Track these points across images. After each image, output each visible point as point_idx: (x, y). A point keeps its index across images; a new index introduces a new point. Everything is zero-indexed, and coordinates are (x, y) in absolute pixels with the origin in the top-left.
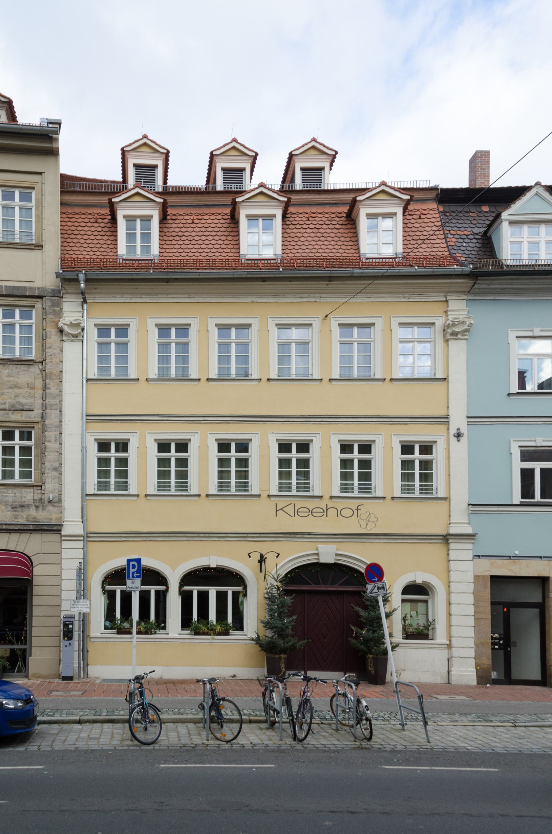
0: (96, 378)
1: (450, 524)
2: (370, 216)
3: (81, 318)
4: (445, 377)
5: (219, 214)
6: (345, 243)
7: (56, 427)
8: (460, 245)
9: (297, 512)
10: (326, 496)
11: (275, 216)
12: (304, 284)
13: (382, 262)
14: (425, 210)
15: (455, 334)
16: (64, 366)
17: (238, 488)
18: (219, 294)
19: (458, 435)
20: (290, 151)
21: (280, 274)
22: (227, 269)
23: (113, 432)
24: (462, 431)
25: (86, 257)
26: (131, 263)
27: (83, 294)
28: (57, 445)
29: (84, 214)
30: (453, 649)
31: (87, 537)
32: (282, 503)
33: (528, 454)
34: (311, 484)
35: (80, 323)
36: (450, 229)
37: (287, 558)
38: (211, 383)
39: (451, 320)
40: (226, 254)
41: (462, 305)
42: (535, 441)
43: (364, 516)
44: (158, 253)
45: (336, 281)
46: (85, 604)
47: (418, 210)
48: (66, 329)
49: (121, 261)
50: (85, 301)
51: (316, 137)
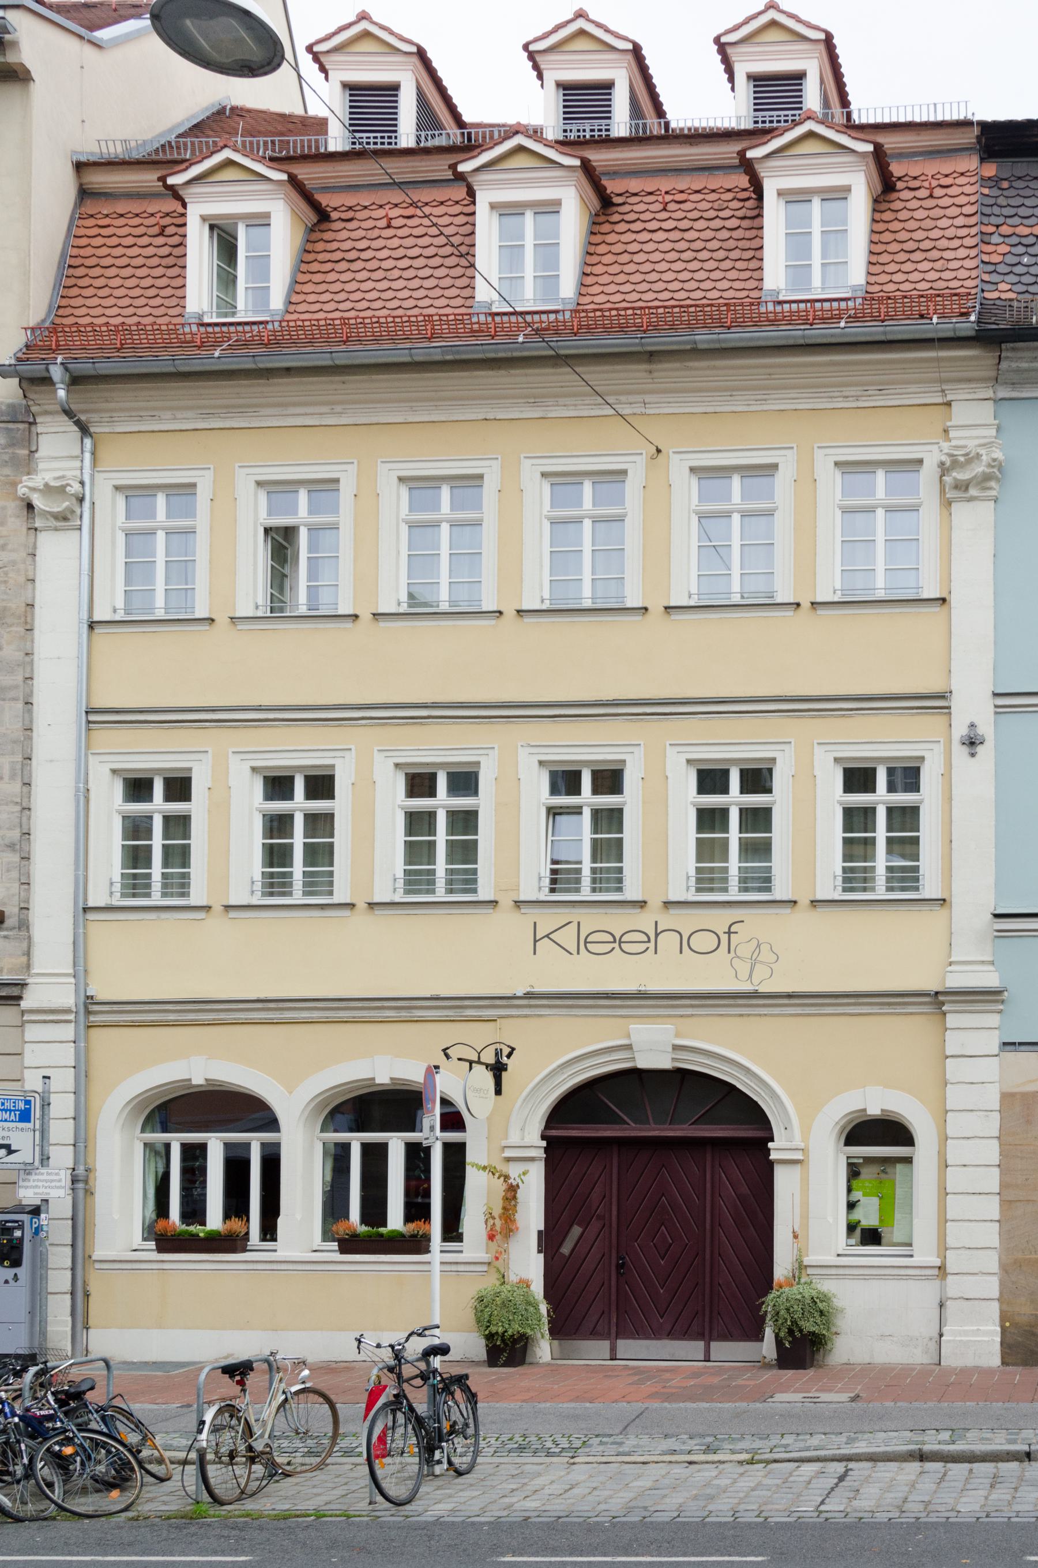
7: (15, 742)
9: (586, 942)
10: (655, 902)
13: (814, 313)
14: (947, 176)
15: (962, 486)
16: (37, 593)
17: (598, 882)
19: (972, 743)
23: (155, 753)
24: (981, 730)
26: (211, 334)
27: (68, 413)
28: (16, 787)
32: (548, 920)
35: (68, 485)
37: (556, 1058)
38: (383, 624)
39: (946, 451)
41: (985, 413)
43: (745, 950)
44: (863, 282)
45: (669, 362)
48: (37, 501)
50: (84, 429)
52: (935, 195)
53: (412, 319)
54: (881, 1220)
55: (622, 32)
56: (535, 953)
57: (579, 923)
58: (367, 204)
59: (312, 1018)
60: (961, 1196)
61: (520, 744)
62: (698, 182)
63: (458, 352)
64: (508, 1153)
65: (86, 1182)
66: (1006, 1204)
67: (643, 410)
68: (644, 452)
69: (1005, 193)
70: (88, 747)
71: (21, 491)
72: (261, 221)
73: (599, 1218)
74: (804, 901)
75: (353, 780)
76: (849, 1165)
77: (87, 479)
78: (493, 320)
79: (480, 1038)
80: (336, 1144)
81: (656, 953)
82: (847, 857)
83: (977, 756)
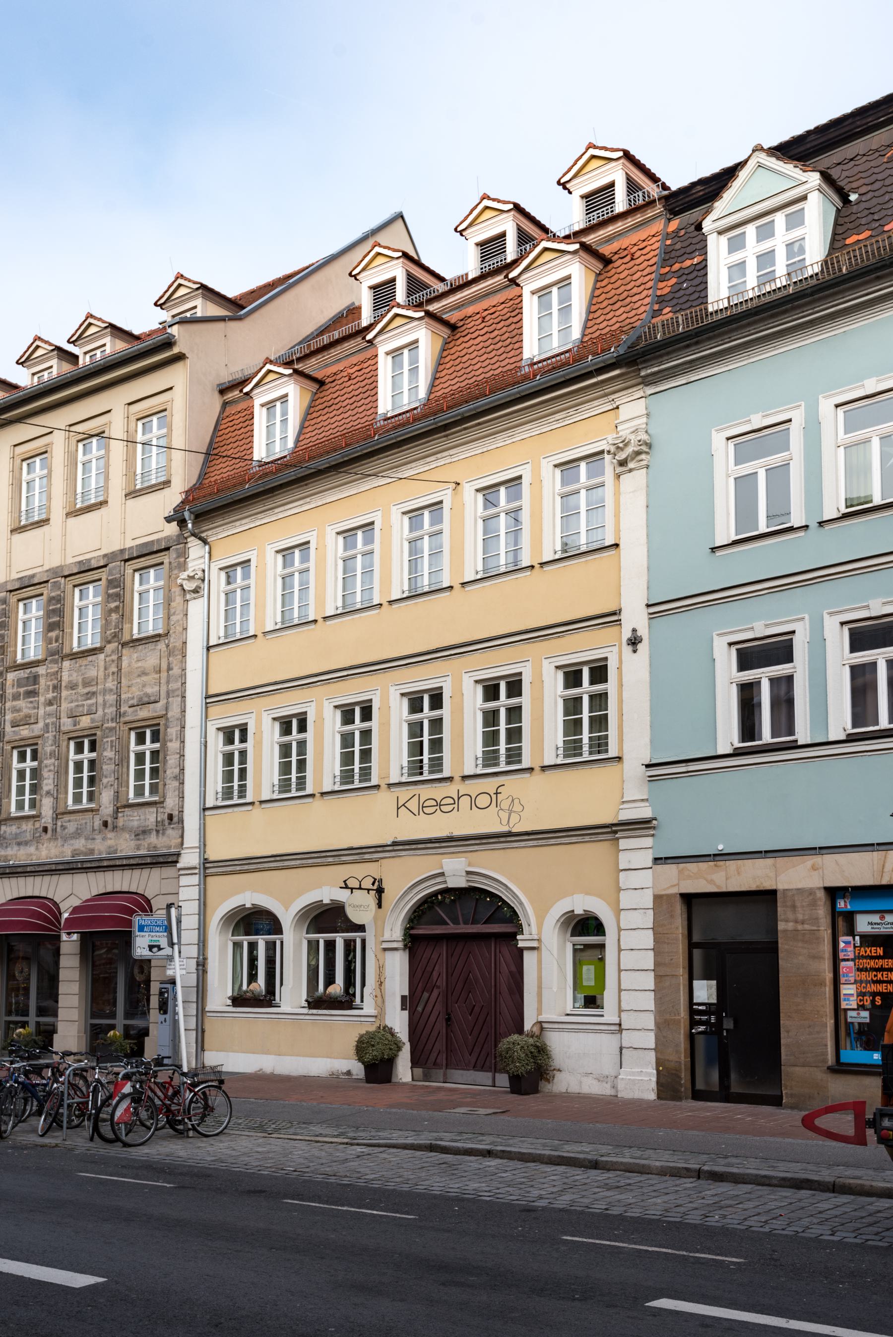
19: (634, 642)
32: (404, 794)
33: (863, 637)
37: (407, 880)
42: (867, 607)
60: (629, 972)
64: (385, 945)
65: (204, 966)
66: (658, 978)
70: (206, 717)
71: (179, 581)
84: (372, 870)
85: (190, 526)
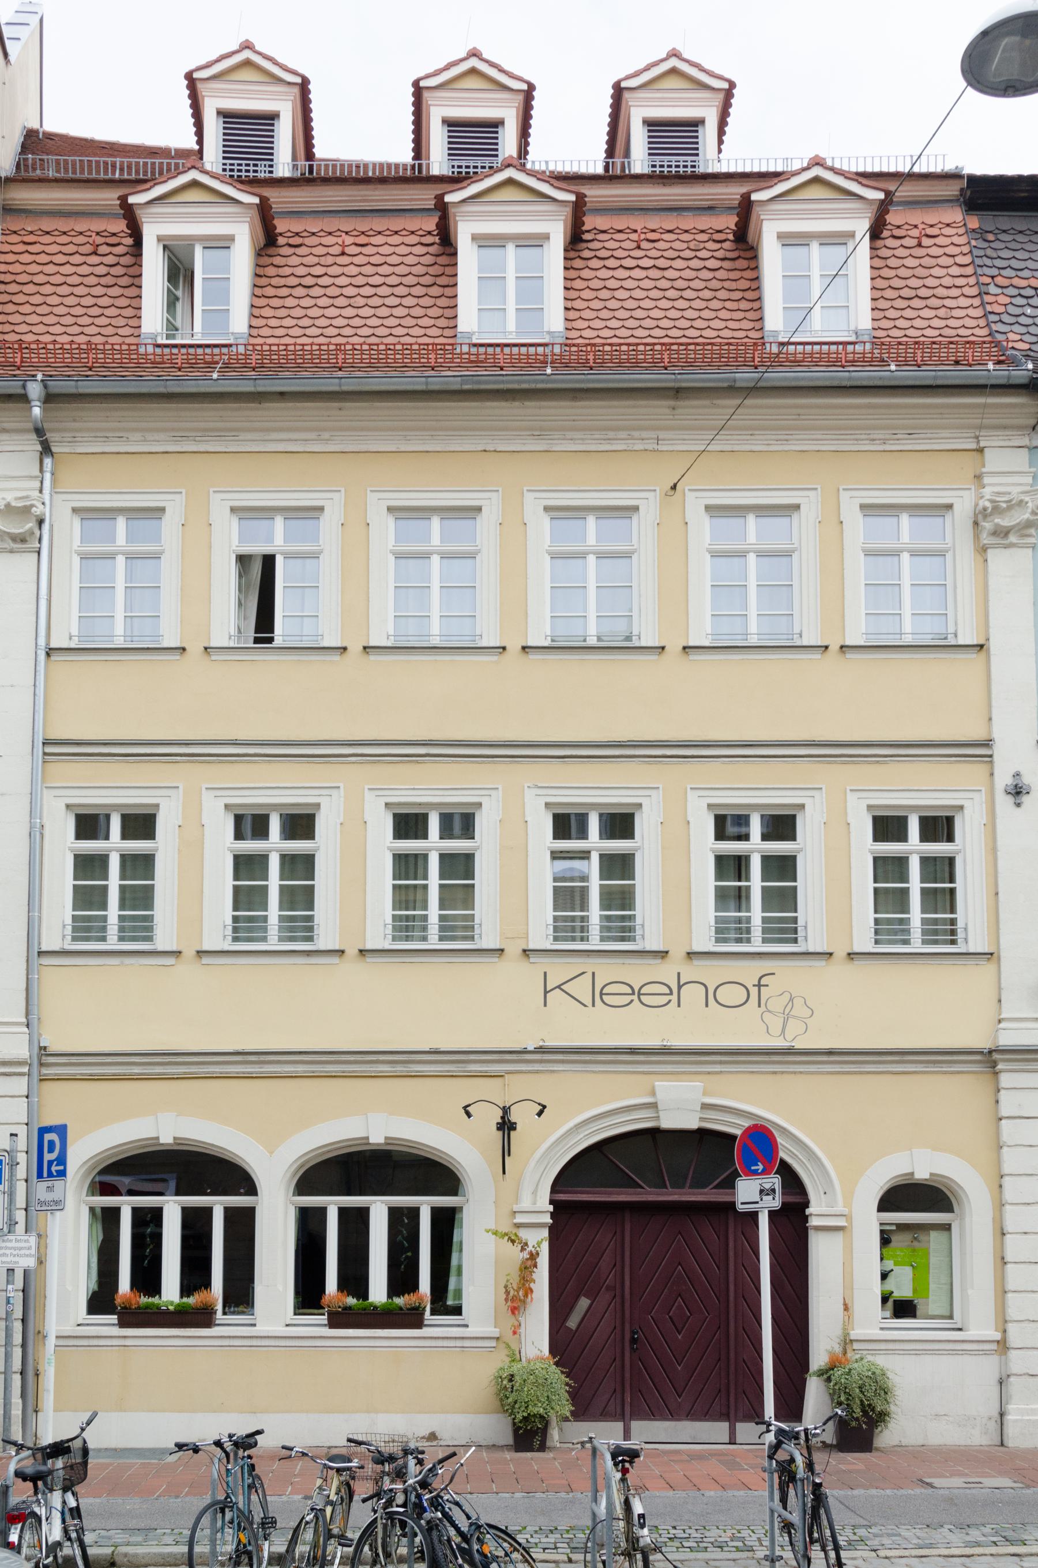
0: (73, 646)
1: (1000, 1021)
2: (483, 241)
3: (37, 493)
4: (981, 642)
5: (413, 233)
6: (729, 305)
8: (1018, 311)
9: (601, 994)
10: (677, 952)
11: (546, 237)
12: (610, 407)
14: (932, 226)
15: (1001, 533)
17: (447, 930)
18: (354, 429)
19: (1017, 792)
20: (615, 80)
21: (547, 382)
22: (360, 369)
23: (115, 789)
25: (77, 339)
27: (39, 432)
29: (65, 233)
30: (1013, 1354)
31: (41, 1065)
32: (559, 971)
34: (801, 922)
35: (32, 506)
36: (994, 272)
39: (988, 497)
40: (629, 333)
41: (1020, 460)
43: (777, 1004)
45: (697, 398)
46: (23, 1245)
47: (916, 226)
49: (150, 349)
50: (46, 449)
51: (680, 48)
52: (642, 246)
53: (116, 347)
54: (915, 1291)
55: (517, 72)
56: (545, 1005)
57: (593, 974)
58: (315, 231)
59: (297, 1072)
60: (1022, 1266)
61: (526, 785)
62: (670, 222)
63: (479, 382)
67: (656, 447)
68: (658, 489)
69: (993, 245)
72: (223, 243)
73: (608, 1288)
74: (840, 953)
75: (342, 820)
76: (882, 1232)
77: (47, 502)
78: (502, 351)
79: (490, 1093)
80: (103, 1209)
81: (679, 1006)
82: (397, 904)
83: (1023, 806)
84: (495, 1091)
85: (37, 411)
